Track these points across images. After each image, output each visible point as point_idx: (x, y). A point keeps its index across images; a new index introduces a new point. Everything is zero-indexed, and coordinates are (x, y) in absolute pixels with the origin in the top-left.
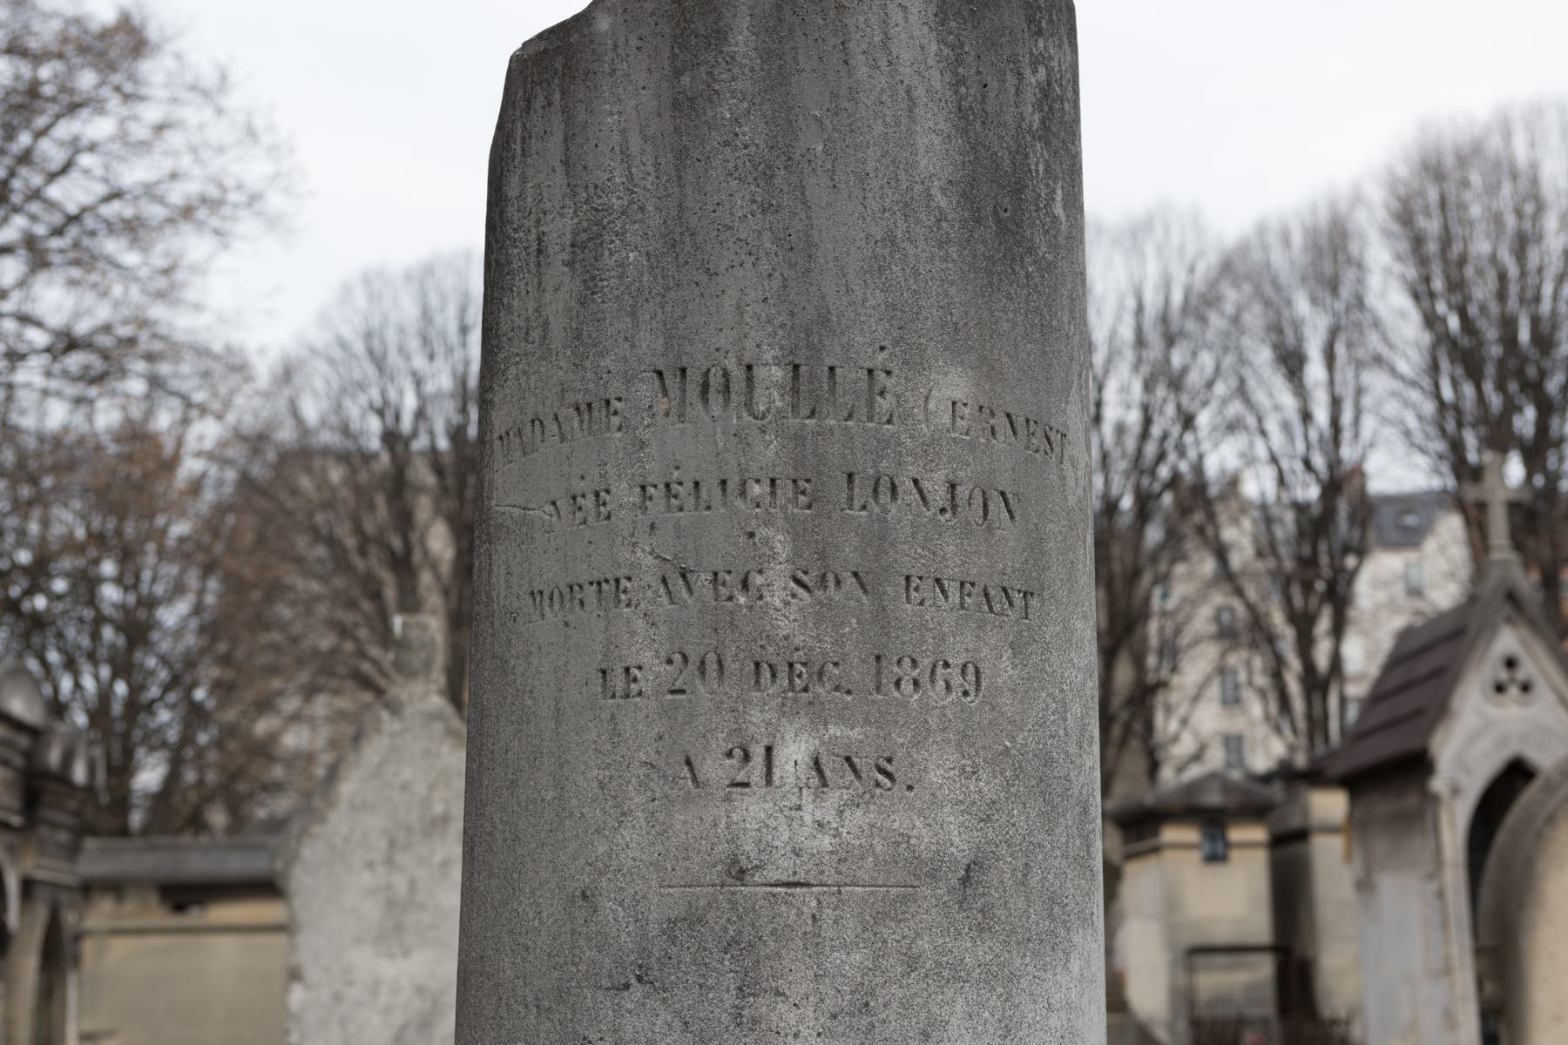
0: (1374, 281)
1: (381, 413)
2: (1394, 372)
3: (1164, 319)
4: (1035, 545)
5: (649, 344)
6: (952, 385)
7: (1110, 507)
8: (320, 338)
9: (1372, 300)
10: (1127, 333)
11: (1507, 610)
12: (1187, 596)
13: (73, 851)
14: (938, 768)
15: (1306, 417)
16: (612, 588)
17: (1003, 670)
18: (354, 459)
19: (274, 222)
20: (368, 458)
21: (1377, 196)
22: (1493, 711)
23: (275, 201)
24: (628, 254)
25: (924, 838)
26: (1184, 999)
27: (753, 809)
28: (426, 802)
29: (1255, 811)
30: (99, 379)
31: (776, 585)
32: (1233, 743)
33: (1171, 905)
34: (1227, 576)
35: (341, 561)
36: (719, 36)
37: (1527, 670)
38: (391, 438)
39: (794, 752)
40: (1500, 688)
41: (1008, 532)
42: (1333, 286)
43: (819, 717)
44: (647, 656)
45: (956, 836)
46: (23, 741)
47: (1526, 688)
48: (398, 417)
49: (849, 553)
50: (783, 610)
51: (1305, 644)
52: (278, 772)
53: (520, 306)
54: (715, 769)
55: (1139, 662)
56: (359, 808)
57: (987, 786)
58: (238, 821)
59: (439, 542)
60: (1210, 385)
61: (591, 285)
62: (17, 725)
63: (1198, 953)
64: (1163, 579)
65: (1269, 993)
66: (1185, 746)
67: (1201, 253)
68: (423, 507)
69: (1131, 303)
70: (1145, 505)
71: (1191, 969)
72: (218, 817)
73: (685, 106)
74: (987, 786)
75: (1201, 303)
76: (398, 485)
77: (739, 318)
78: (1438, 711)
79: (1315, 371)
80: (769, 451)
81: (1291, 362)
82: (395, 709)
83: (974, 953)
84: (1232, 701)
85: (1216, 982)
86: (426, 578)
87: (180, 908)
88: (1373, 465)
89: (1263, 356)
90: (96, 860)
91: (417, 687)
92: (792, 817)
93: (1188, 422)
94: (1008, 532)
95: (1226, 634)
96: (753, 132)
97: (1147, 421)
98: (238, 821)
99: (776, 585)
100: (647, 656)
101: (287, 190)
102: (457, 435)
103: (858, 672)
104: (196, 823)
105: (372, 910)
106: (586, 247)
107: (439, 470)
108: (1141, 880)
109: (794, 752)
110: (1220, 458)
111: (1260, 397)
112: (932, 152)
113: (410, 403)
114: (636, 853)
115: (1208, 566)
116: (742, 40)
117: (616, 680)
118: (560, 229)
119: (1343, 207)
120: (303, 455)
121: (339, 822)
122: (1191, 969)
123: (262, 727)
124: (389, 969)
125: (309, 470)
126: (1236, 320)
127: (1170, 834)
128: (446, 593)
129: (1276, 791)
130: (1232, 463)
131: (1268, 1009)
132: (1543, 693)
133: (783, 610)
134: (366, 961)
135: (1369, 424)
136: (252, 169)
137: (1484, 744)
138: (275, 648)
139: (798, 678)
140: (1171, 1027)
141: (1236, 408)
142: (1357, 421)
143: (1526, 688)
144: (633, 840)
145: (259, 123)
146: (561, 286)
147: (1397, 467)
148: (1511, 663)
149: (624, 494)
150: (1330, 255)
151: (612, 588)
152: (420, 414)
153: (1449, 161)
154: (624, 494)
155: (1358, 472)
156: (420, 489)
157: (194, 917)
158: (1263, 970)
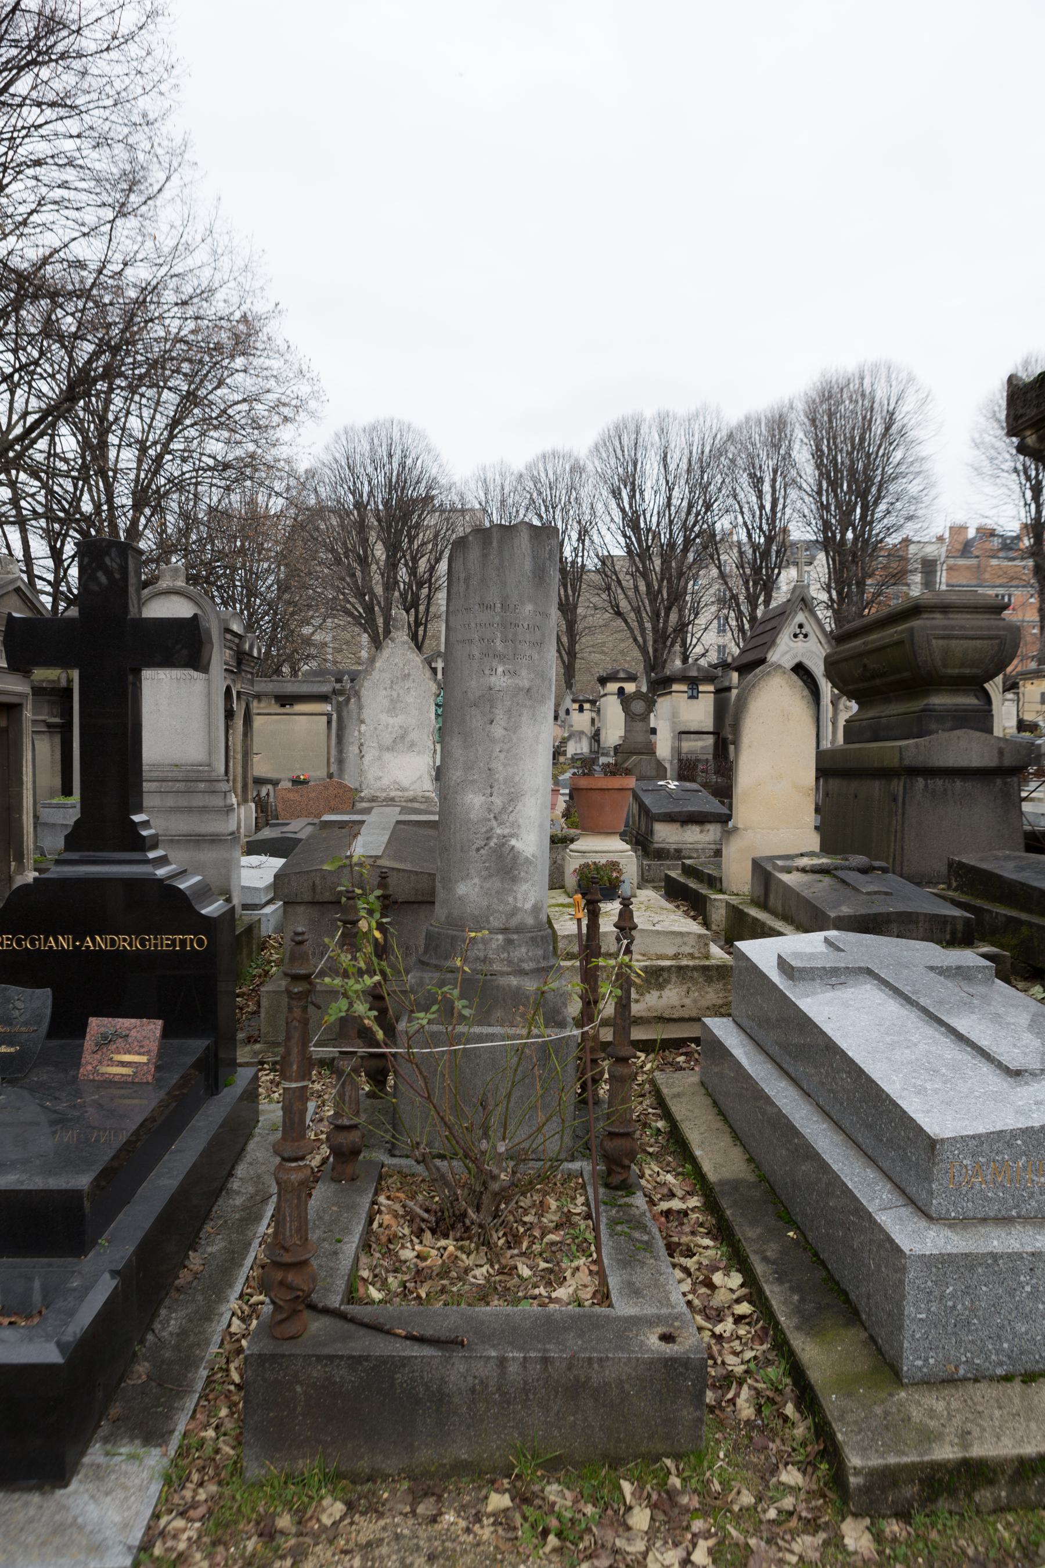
0: (796, 446)
1: (353, 494)
2: (800, 488)
3: (701, 460)
4: (543, 635)
5: (477, 599)
6: (529, 607)
7: (672, 545)
8: (327, 458)
9: (794, 454)
10: (684, 466)
11: (801, 605)
12: (705, 585)
13: (252, 682)
14: (524, 673)
15: (762, 507)
16: (471, 641)
17: (536, 656)
18: (341, 511)
19: (312, 414)
20: (348, 513)
21: (800, 406)
22: (792, 644)
23: (312, 404)
24: (474, 582)
25: (521, 684)
26: (677, 751)
27: (493, 679)
28: (403, 670)
29: (710, 679)
30: (236, 480)
31: (498, 642)
32: (721, 649)
33: (675, 714)
34: (722, 575)
35: (338, 561)
36: (491, 543)
37: (807, 629)
38: (359, 505)
39: (500, 670)
40: (796, 636)
41: (538, 633)
42: (777, 447)
43: (504, 664)
44: (476, 653)
45: (526, 684)
46: (237, 640)
47: (806, 636)
48: (361, 496)
49: (510, 636)
50: (499, 645)
51: (754, 606)
52: (313, 651)
53: (454, 589)
54: (487, 672)
55: (681, 611)
56: (382, 671)
57: (532, 676)
58: (295, 672)
59: (380, 551)
60: (720, 490)
61: (468, 587)
62: (235, 634)
63: (684, 733)
64: (695, 578)
65: (711, 750)
66: (699, 650)
67: (719, 430)
68: (373, 536)
69: (686, 452)
70: (688, 542)
71: (680, 740)
72: (286, 669)
73: (485, 556)
74: (532, 676)
75: (719, 453)
76: (362, 527)
77: (493, 595)
78: (772, 643)
79: (767, 488)
80: (497, 619)
81: (757, 482)
82: (393, 640)
83: (528, 703)
84: (721, 631)
85: (689, 745)
86: (374, 567)
87: (283, 706)
88: (791, 527)
89: (744, 479)
90: (263, 686)
91: (399, 633)
92: (499, 680)
93: (708, 506)
94: (538, 633)
95: (721, 601)
96: (496, 561)
97: (690, 506)
98: (295, 672)
99: (498, 642)
100: (476, 653)
101: (317, 399)
102: (387, 503)
103: (511, 657)
104: (278, 671)
105: (386, 702)
106: (467, 580)
107: (379, 521)
108: (663, 705)
109: (500, 670)
110: (723, 524)
111: (741, 496)
112: (528, 565)
113: (366, 489)
114: (474, 685)
115: (715, 572)
116: (495, 544)
117: (471, 657)
118: (462, 576)
119: (785, 410)
120: (320, 511)
121: (376, 674)
122: (680, 740)
123: (307, 630)
124: (391, 720)
125: (323, 519)
126: (733, 461)
127: (675, 687)
128: (382, 575)
129: (719, 672)
130: (727, 526)
131: (710, 757)
132: (812, 637)
133: (499, 645)
134: (384, 718)
135: (788, 511)
136: (303, 389)
137: (788, 656)
138: (309, 597)
139: (501, 658)
140: (671, 762)
141: (731, 501)
142: (784, 507)
143: (806, 636)
144: (474, 683)
145: (305, 368)
146: (462, 587)
147: (801, 531)
148: (801, 626)
149: (473, 625)
150: (778, 428)
151: (471, 641)
152: (371, 493)
153: (836, 389)
154: (473, 625)
155: (785, 530)
156: (371, 528)
157: (287, 709)
158: (710, 740)
